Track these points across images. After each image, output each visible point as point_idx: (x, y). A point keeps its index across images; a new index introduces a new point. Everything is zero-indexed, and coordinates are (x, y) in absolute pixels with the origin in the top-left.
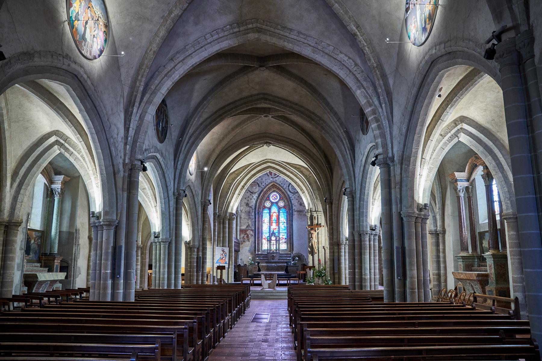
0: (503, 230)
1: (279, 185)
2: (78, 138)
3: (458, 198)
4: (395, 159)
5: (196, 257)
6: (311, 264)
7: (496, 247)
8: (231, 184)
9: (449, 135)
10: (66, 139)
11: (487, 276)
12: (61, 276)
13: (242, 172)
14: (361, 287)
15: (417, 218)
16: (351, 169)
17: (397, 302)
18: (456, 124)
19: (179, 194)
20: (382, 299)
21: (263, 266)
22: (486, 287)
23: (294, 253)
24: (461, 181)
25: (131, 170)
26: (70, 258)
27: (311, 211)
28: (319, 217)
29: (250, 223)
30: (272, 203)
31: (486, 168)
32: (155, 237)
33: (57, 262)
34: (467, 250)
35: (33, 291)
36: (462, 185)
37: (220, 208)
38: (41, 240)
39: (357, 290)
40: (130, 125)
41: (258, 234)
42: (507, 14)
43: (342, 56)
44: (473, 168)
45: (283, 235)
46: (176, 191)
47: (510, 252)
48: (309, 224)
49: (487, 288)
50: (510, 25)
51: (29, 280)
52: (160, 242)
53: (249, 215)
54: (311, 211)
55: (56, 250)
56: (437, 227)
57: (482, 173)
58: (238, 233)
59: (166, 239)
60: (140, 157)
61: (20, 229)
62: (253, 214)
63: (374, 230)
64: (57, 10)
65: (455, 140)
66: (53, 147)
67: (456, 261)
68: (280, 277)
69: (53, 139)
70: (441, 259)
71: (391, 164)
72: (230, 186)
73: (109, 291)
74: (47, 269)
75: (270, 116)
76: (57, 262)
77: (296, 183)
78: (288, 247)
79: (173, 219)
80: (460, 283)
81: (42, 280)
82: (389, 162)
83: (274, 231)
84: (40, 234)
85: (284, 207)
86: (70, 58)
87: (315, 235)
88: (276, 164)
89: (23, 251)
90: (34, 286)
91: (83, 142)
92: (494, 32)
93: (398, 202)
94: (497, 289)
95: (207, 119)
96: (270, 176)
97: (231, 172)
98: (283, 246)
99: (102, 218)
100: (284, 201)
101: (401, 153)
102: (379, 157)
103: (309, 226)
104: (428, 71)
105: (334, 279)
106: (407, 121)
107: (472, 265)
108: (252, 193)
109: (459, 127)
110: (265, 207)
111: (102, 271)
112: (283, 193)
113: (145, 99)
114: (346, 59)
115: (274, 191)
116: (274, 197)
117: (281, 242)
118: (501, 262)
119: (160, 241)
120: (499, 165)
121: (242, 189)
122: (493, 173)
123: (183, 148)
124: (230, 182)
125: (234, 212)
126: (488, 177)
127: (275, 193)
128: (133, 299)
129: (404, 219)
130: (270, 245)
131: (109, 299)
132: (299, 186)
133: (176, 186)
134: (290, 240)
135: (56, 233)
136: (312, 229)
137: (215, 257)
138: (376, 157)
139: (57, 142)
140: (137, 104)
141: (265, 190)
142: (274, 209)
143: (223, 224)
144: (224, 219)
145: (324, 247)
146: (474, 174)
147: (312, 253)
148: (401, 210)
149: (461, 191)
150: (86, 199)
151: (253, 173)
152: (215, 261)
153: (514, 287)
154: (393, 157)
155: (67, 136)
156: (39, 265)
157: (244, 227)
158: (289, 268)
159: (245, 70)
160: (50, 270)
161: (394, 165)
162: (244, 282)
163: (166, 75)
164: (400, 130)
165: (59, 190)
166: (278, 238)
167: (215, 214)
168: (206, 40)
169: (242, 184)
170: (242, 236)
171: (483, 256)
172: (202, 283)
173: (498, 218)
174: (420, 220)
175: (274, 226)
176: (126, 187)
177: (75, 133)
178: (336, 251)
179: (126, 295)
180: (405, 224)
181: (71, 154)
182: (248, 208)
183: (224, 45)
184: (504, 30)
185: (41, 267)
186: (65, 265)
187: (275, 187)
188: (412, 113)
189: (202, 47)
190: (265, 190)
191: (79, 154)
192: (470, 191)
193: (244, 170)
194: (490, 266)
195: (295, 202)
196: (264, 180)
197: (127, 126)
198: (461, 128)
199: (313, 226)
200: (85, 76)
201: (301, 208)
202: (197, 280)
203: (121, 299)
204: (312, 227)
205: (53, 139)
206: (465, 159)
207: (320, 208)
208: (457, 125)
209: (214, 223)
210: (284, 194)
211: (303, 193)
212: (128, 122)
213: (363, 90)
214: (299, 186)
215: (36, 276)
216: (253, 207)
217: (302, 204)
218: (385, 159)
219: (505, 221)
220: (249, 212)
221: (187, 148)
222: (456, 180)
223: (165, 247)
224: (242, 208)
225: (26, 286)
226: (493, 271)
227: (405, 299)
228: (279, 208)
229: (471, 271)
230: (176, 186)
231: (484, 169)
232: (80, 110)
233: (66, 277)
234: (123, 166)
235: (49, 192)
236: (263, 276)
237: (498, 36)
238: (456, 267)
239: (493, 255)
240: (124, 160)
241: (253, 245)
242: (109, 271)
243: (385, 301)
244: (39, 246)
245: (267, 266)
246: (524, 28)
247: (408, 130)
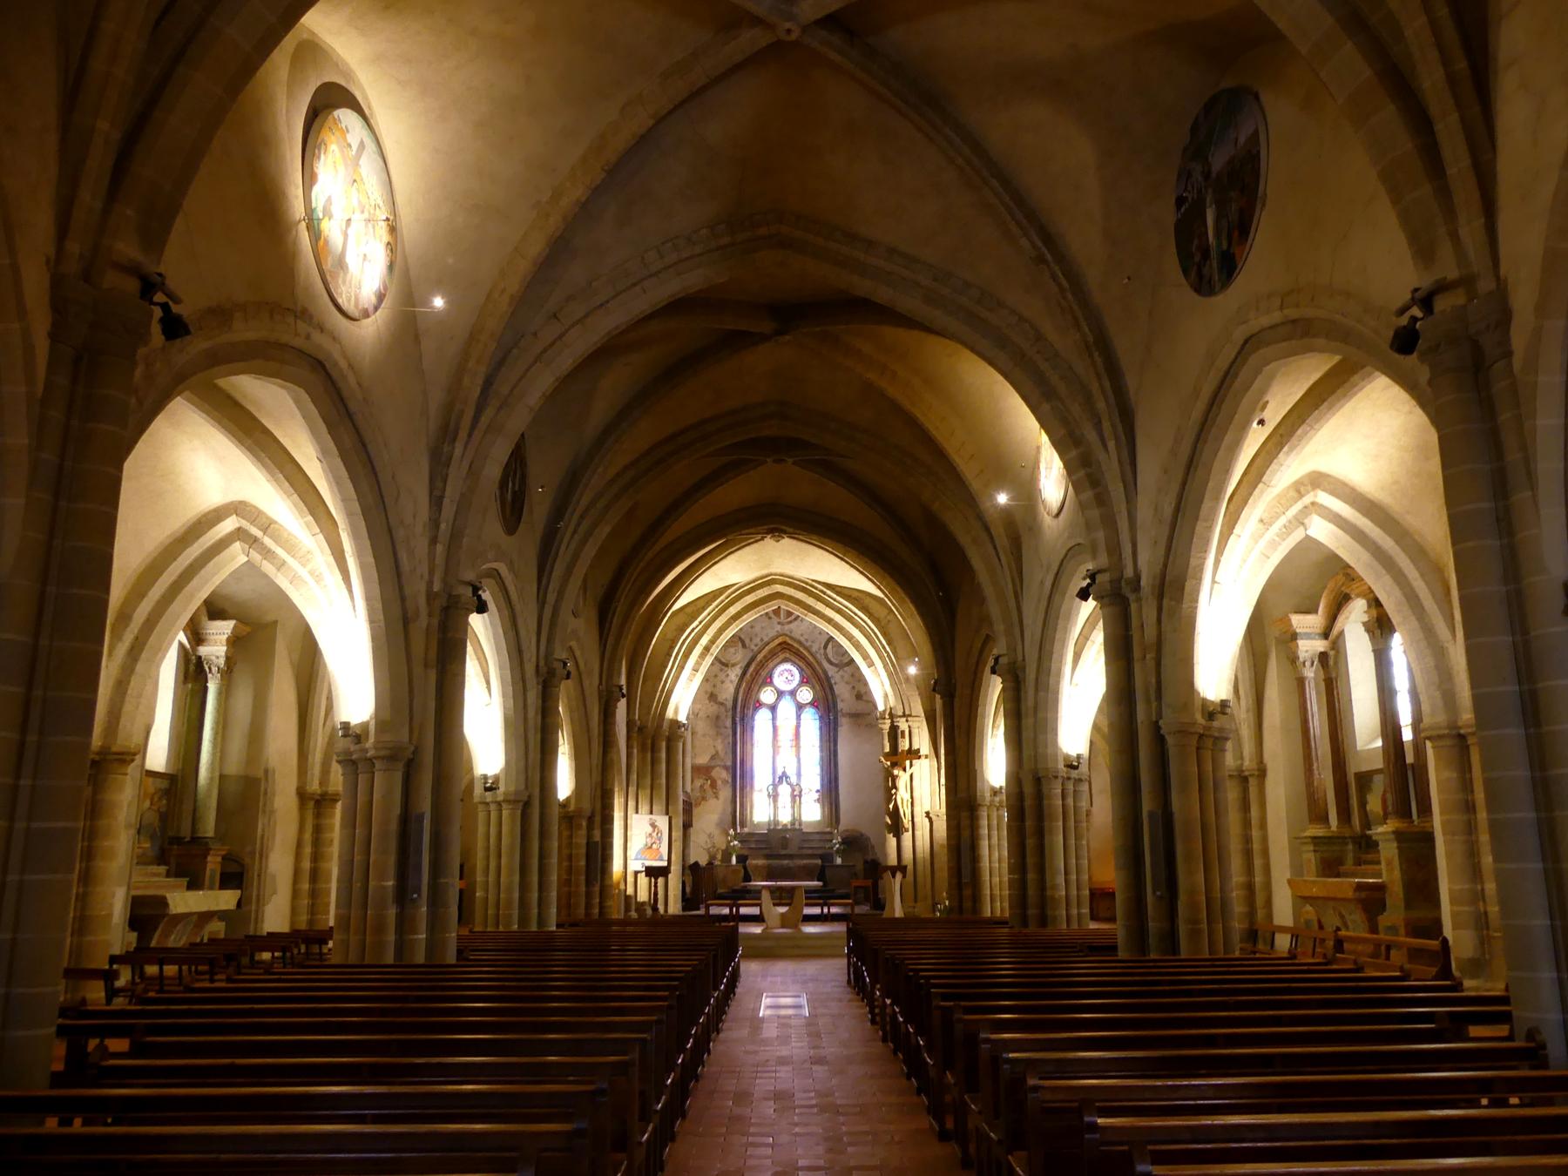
0: (1420, 768)
1: (800, 643)
2: (307, 525)
3: (1301, 682)
4: (1143, 583)
5: (584, 841)
6: (892, 860)
7: (1403, 812)
8: (674, 642)
9: (1283, 520)
10: (268, 525)
11: (1380, 888)
12: (226, 900)
13: (704, 609)
14: (1043, 921)
15: (1201, 736)
16: (1012, 603)
17: (1153, 956)
18: (1299, 492)
19: (551, 673)
20: (1113, 949)
21: (757, 867)
22: (1380, 918)
23: (841, 828)
24: (1308, 636)
25: (446, 610)
26: (248, 849)
27: (892, 716)
28: (915, 731)
29: (720, 748)
30: (780, 694)
31: (1375, 603)
32: (487, 789)
33: (213, 863)
34: (1324, 819)
35: (153, 944)
36: (1309, 647)
37: (646, 706)
38: (168, 800)
39: (1032, 928)
40: (444, 490)
41: (742, 777)
42: (1446, 251)
44: (1339, 604)
45: (812, 780)
46: (542, 663)
47: (1443, 824)
48: (887, 749)
49: (1384, 920)
50: (1452, 274)
51: (146, 914)
52: (499, 804)
53: (717, 727)
54: (892, 716)
55: (209, 827)
56: (1242, 758)
57: (1365, 618)
59: (517, 793)
60: (470, 576)
61: (131, 769)
62: (729, 723)
63: (1076, 768)
64: (284, 194)
65: (1298, 535)
66: (227, 546)
67: (1295, 852)
68: (813, 897)
69: (229, 525)
70: (1256, 846)
71: (1132, 597)
72: (672, 648)
73: (391, 937)
74: (185, 881)
75: (790, 461)
76: (213, 863)
77: (850, 638)
79: (534, 740)
80: (1309, 908)
82: (1126, 591)
83: (786, 772)
84: (164, 784)
85: (813, 704)
86: (311, 317)
87: (903, 779)
88: (797, 587)
90: (156, 928)
91: (321, 536)
92: (1416, 290)
93: (1153, 697)
94: (1408, 923)
95: (626, 468)
96: (775, 620)
97: (675, 607)
99: (372, 740)
100: (813, 688)
101: (1158, 569)
102: (1099, 578)
103: (887, 756)
104: (1234, 362)
105: (961, 901)
106: (1175, 487)
107: (1340, 861)
108: (726, 665)
109: (1307, 500)
110: (759, 705)
111: (372, 884)
112: (809, 664)
113: (484, 420)
115: (785, 660)
116: (786, 675)
118: (1418, 849)
119: (500, 798)
120: (1412, 598)
121: (703, 656)
122: (1395, 619)
123: (563, 547)
124: (670, 636)
125: (682, 718)
126: (1380, 627)
127: (788, 666)
128: (451, 958)
129: (1170, 740)
130: (776, 808)
131: (389, 958)
132: (858, 646)
133: (543, 648)
135: (211, 779)
136: (894, 765)
137: (638, 842)
138: (1093, 576)
139: (239, 534)
140: (463, 434)
141: (760, 657)
142: (787, 708)
143: (653, 751)
144: (657, 741)
145: (928, 814)
146: (1340, 619)
147: (897, 828)
148: (1159, 715)
149: (1308, 664)
150: (802, 729)
151: (733, 610)
152: (631, 853)
153: (1454, 915)
154: (1138, 577)
155: (268, 518)
156: (162, 869)
157: (703, 760)
158: (828, 872)
159: (737, 341)
160: (194, 885)
161: (1139, 600)
162: (714, 911)
163: (537, 359)
164: (1156, 509)
165: (222, 662)
167: (630, 724)
169: (704, 641)
170: (698, 783)
171: (1370, 837)
172: (601, 913)
173: (1407, 735)
174: (1209, 743)
176: (433, 654)
177: (300, 512)
178: (965, 822)
179: (433, 946)
180: (1172, 751)
181: (281, 565)
182: (715, 707)
183: (692, 280)
184: (1441, 287)
185: (168, 875)
186: (233, 868)
187: (788, 649)
188: (1190, 465)
189: (634, 285)
190: (760, 657)
191: (304, 565)
192: (1331, 663)
193: (708, 604)
194: (1389, 863)
195: (842, 691)
197: (437, 493)
198: (1313, 504)
199: (899, 757)
200: (343, 364)
201: (860, 707)
202: (588, 906)
203: (420, 958)
204: (895, 759)
205: (229, 525)
206: (1317, 583)
207: (918, 708)
208: (1301, 496)
209: (629, 747)
210: (813, 669)
211: (871, 664)
212: (439, 484)
214: (858, 646)
215: (162, 902)
216: (730, 704)
217: (862, 693)
218: (1116, 583)
219: (1429, 744)
220: (718, 717)
221: (573, 546)
222: (1294, 636)
223: (512, 816)
226: (1397, 874)
227: (1175, 949)
228: (800, 707)
229: (1338, 876)
230: (543, 648)
231: (1369, 606)
232: (324, 455)
233: (239, 904)
234: (428, 600)
235: (192, 668)
236: (765, 895)
237: (1426, 301)
238: (1297, 868)
239: (1399, 835)
240: (430, 583)
241: (729, 810)
242: (391, 883)
243: (1122, 954)
245: (769, 866)
246: (1485, 285)
247: (1177, 509)
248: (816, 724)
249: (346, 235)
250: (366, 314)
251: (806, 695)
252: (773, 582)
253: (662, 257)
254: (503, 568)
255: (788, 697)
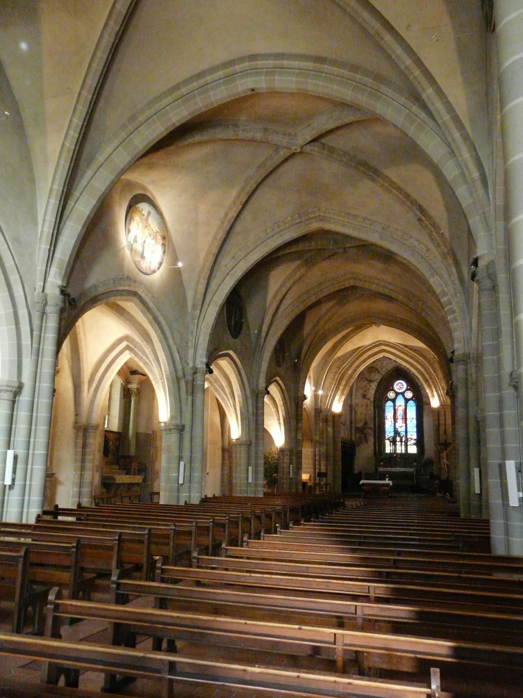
12: (138, 479)
30: (397, 394)
43: (412, 241)
45: (413, 434)
55: (133, 451)
58: (353, 432)
76: (134, 465)
78: (418, 450)
81: (120, 482)
84: (116, 436)
86: (130, 279)
88: (391, 347)
89: (101, 453)
98: (413, 450)
108: (370, 381)
114: (416, 243)
116: (400, 385)
117: (409, 443)
134: (420, 442)
142: (400, 401)
166: (404, 439)
168: (267, 234)
170: (358, 435)
175: (400, 423)
185: (119, 469)
196: (385, 364)
213: (437, 277)
215: (114, 479)
224: (358, 400)
225: (105, 488)
228: (407, 400)
233: (144, 481)
244: (117, 448)
248: (414, 408)
249: (143, 247)
250: (154, 272)
251: (409, 395)
252: (380, 344)
253: (273, 230)
254: (231, 352)
255: (400, 396)
